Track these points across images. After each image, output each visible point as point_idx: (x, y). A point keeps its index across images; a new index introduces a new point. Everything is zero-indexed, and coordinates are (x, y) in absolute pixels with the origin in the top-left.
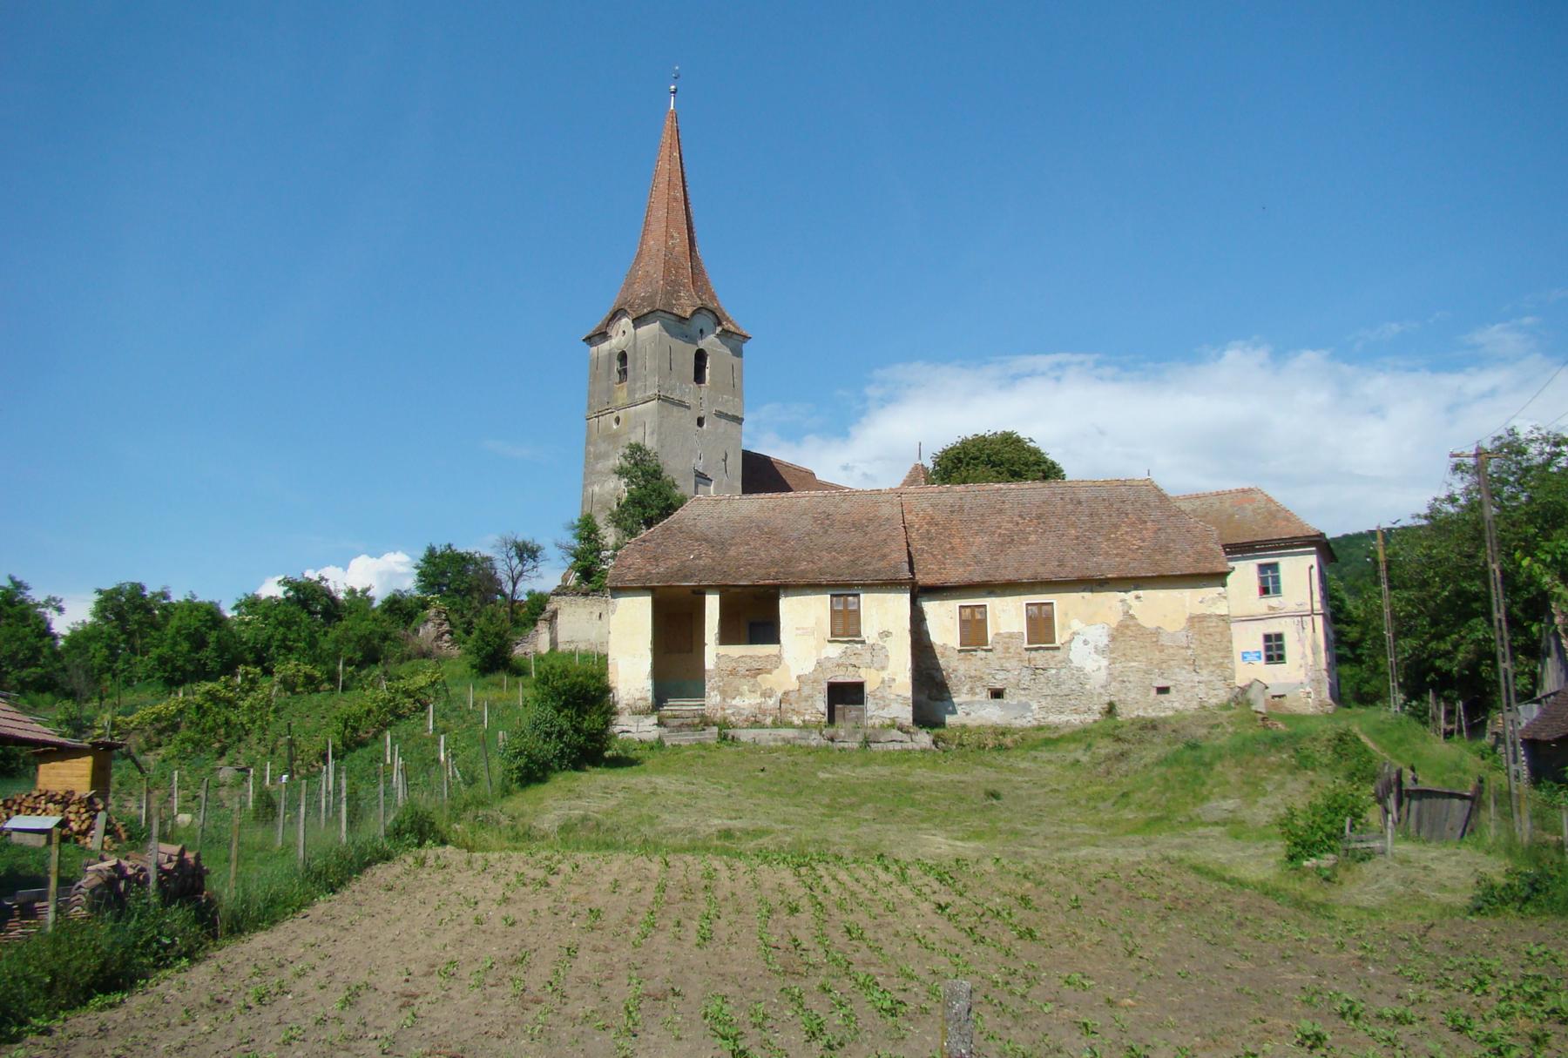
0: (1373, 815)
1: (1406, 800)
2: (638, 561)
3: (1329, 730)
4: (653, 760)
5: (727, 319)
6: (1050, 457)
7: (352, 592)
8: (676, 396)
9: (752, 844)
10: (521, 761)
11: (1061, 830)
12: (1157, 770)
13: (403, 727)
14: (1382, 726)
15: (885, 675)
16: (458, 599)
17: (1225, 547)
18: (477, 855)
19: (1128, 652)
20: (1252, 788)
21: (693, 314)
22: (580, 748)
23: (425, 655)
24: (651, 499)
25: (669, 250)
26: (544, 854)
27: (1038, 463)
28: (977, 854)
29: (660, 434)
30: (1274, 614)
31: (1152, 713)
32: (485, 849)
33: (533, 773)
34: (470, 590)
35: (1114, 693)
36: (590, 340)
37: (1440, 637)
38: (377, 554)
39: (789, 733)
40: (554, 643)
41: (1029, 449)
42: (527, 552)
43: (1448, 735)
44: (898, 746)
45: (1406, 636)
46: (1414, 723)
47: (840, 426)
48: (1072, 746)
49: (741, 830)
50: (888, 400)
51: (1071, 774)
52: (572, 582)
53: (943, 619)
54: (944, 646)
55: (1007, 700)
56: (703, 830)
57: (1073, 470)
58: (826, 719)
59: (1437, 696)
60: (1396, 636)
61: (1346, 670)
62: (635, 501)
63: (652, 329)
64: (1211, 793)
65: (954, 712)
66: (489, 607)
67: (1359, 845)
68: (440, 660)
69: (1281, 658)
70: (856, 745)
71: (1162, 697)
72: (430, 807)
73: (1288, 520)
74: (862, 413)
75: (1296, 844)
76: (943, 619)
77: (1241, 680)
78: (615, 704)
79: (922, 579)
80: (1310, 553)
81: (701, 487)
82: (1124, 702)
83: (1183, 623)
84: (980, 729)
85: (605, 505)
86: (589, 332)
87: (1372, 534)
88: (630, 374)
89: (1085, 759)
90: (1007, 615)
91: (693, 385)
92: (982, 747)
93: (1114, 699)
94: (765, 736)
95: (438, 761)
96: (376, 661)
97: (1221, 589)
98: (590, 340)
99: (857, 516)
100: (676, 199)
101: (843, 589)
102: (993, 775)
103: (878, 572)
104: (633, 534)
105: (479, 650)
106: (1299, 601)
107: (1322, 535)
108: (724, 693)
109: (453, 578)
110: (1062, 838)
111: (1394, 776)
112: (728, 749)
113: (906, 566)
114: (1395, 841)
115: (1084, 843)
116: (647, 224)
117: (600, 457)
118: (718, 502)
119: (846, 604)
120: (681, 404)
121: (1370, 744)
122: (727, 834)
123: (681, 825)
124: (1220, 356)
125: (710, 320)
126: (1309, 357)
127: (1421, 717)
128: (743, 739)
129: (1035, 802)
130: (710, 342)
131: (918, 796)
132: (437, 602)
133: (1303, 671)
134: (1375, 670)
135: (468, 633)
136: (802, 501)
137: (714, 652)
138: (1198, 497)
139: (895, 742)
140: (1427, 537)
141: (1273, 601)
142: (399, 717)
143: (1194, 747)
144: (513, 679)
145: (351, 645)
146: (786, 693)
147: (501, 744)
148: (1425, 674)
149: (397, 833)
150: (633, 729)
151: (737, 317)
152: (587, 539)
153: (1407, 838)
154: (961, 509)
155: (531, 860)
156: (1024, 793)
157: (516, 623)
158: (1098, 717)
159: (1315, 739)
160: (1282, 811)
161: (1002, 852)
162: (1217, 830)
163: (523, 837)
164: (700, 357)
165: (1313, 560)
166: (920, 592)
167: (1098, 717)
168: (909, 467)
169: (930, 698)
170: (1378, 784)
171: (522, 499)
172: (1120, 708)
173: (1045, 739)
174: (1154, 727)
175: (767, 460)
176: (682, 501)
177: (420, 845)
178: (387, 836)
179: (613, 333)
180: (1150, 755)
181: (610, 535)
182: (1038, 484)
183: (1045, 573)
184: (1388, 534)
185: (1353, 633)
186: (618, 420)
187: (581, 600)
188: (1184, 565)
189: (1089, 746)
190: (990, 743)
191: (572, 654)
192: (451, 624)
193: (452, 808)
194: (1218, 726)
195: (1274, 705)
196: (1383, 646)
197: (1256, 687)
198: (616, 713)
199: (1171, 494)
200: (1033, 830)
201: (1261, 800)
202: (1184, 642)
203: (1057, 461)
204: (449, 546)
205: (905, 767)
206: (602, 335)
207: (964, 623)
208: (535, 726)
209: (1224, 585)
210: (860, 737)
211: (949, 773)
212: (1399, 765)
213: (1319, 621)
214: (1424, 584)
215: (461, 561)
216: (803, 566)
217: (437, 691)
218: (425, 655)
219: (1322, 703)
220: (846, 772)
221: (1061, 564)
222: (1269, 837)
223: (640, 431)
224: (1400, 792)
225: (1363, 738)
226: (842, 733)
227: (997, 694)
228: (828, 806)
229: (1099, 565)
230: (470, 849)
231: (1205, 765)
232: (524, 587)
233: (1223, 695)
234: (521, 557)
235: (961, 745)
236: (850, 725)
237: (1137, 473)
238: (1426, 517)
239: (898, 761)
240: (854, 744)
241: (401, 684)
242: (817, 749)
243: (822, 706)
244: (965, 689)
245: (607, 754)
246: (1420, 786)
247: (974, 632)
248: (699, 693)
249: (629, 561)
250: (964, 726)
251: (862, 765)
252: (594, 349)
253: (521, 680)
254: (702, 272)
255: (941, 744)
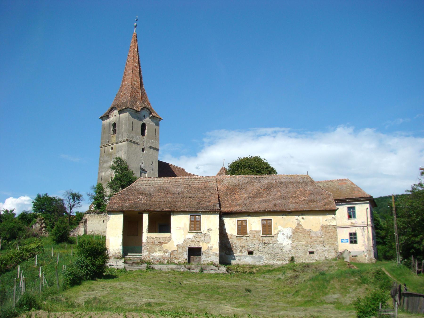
0: (390, 302)
1: (403, 297)
2: (118, 201)
3: (373, 269)
4: (122, 276)
5: (154, 112)
6: (271, 166)
7: (7, 211)
8: (134, 140)
9: (158, 308)
10: (71, 277)
11: (273, 304)
12: (309, 282)
13: (25, 264)
14: (391, 268)
15: (209, 245)
16: (49, 214)
17: (335, 200)
18: (52, 313)
19: (299, 238)
20: (345, 290)
21: (141, 109)
22: (94, 272)
23: (35, 236)
24: (124, 178)
25: (133, 86)
26: (79, 312)
27: (267, 168)
28: (242, 313)
29: (128, 154)
30: (353, 225)
31: (307, 261)
32: (55, 311)
33: (75, 281)
34: (53, 211)
35: (293, 253)
36: (102, 118)
37: (416, 236)
38: (16, 197)
39: (173, 266)
40: (85, 231)
41: (264, 163)
42: (76, 197)
43: (419, 273)
44: (213, 272)
45: (403, 235)
46: (406, 268)
47: (194, 152)
48: (278, 273)
49: (154, 303)
50: (212, 143)
51: (277, 283)
52: (93, 208)
53: (231, 225)
54: (231, 235)
55: (254, 255)
56: (140, 303)
57: (280, 170)
58: (187, 261)
59: (415, 258)
60: (399, 235)
61: (380, 247)
62: (118, 179)
63: (126, 115)
64: (329, 292)
65: (235, 259)
66: (61, 217)
67: (385, 313)
68: (41, 238)
69: (356, 242)
70: (198, 271)
71: (311, 255)
72: (34, 295)
73: (359, 191)
74: (202, 148)
75: (361, 312)
76: (231, 225)
77: (340, 250)
78: (108, 255)
79: (224, 210)
80: (367, 203)
81: (143, 174)
82: (297, 257)
83: (319, 228)
84: (244, 266)
85: (107, 180)
86: (102, 115)
87: (390, 197)
88: (117, 131)
89: (282, 278)
90: (254, 224)
91: (141, 136)
92: (244, 272)
93: (293, 255)
94: (164, 267)
95: (38, 276)
96: (15, 238)
97: (333, 216)
98: (102, 118)
99: (201, 185)
100: (136, 67)
101: (195, 213)
102: (248, 283)
103: (207, 207)
104: (116, 191)
105: (56, 234)
106: (363, 221)
107: (371, 197)
108: (149, 251)
109: (47, 206)
110: (273, 307)
111: (398, 288)
112: (150, 272)
113: (218, 205)
114: (399, 312)
115: (281, 309)
116: (125, 75)
117: (105, 162)
118: (149, 180)
119: (195, 218)
120: (136, 143)
121: (389, 275)
122: (149, 304)
123: (131, 301)
124: (334, 130)
125: (148, 112)
126: (368, 130)
127: (408, 265)
128: (156, 268)
129: (264, 294)
130: (147, 120)
131: (221, 291)
132: (41, 215)
133: (364, 247)
134: (391, 247)
135: (52, 227)
136: (180, 180)
137: (146, 235)
138: (326, 182)
139: (213, 270)
140: (411, 199)
141: (353, 221)
142: (24, 260)
143: (323, 274)
144: (69, 245)
145: (5, 232)
146: (172, 251)
147: (64, 270)
148: (410, 249)
149: (20, 306)
150: (115, 264)
151: (158, 111)
152: (99, 193)
153: (403, 311)
154: (239, 184)
155: (73, 315)
156: (259, 290)
157: (71, 224)
158: (287, 262)
159: (368, 273)
160: (355, 299)
161: (251, 312)
162: (331, 306)
163: (71, 306)
164: (144, 126)
165: (368, 206)
166: (223, 215)
167: (287, 262)
168: (220, 168)
169: (226, 254)
170: (392, 290)
171: (74, 178)
172: (296, 259)
173: (268, 270)
174: (308, 266)
175: (167, 164)
176: (135, 179)
177: (29, 310)
178: (16, 306)
179: (111, 116)
180: (307, 277)
181: (108, 191)
182: (267, 176)
183: (269, 209)
184: (396, 197)
185: (383, 233)
186: (112, 148)
187: (96, 215)
188: (320, 206)
189: (284, 273)
190: (248, 271)
191: (92, 236)
192: (46, 224)
193: (44, 295)
194: (332, 266)
195: (353, 259)
196: (394, 238)
197: (346, 252)
198: (108, 258)
199: (315, 180)
200: (263, 304)
201: (348, 295)
202: (320, 235)
203: (274, 167)
204: (46, 194)
205: (216, 280)
206: (106, 116)
207: (239, 226)
208: (77, 263)
209: (335, 214)
210: (199, 268)
211: (232, 282)
212: (400, 283)
213: (370, 229)
214: (410, 216)
215: (51, 200)
216: (180, 204)
217: (39, 250)
218: (35, 236)
219: (371, 259)
220: (194, 281)
221: (275, 205)
222: (351, 309)
223: (120, 152)
224: (400, 294)
225: (387, 273)
226: (193, 266)
227: (250, 253)
228: (187, 294)
229: (289, 206)
230: (49, 311)
231: (327, 281)
232: (75, 210)
233: (333, 255)
234: (74, 200)
235: (237, 272)
236: (196, 264)
237: (303, 172)
238: (411, 191)
239: (213, 277)
240: (197, 271)
241: (25, 247)
242: (184, 272)
243: (186, 256)
244: (239, 251)
245: (105, 274)
246: (408, 292)
247: (242, 230)
248: (140, 251)
249: (115, 201)
250: (238, 265)
251: (200, 279)
252: (104, 122)
253: (72, 245)
254: (145, 94)
255: (229, 271)
